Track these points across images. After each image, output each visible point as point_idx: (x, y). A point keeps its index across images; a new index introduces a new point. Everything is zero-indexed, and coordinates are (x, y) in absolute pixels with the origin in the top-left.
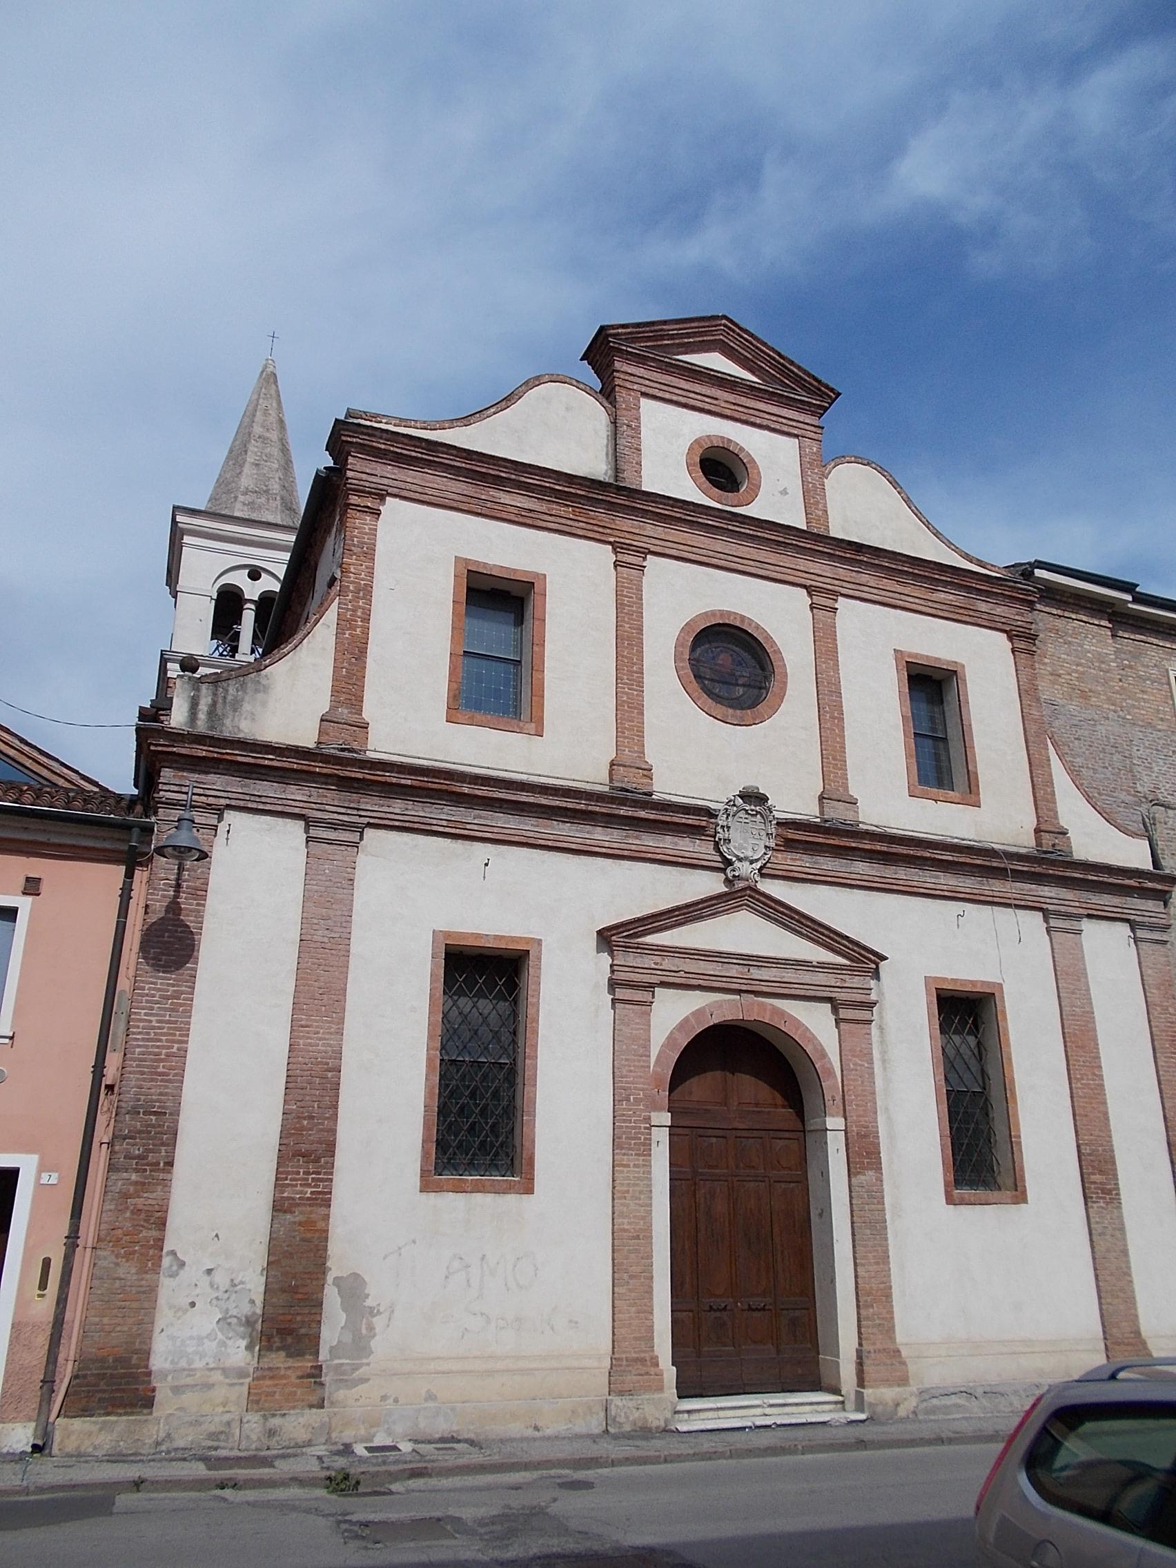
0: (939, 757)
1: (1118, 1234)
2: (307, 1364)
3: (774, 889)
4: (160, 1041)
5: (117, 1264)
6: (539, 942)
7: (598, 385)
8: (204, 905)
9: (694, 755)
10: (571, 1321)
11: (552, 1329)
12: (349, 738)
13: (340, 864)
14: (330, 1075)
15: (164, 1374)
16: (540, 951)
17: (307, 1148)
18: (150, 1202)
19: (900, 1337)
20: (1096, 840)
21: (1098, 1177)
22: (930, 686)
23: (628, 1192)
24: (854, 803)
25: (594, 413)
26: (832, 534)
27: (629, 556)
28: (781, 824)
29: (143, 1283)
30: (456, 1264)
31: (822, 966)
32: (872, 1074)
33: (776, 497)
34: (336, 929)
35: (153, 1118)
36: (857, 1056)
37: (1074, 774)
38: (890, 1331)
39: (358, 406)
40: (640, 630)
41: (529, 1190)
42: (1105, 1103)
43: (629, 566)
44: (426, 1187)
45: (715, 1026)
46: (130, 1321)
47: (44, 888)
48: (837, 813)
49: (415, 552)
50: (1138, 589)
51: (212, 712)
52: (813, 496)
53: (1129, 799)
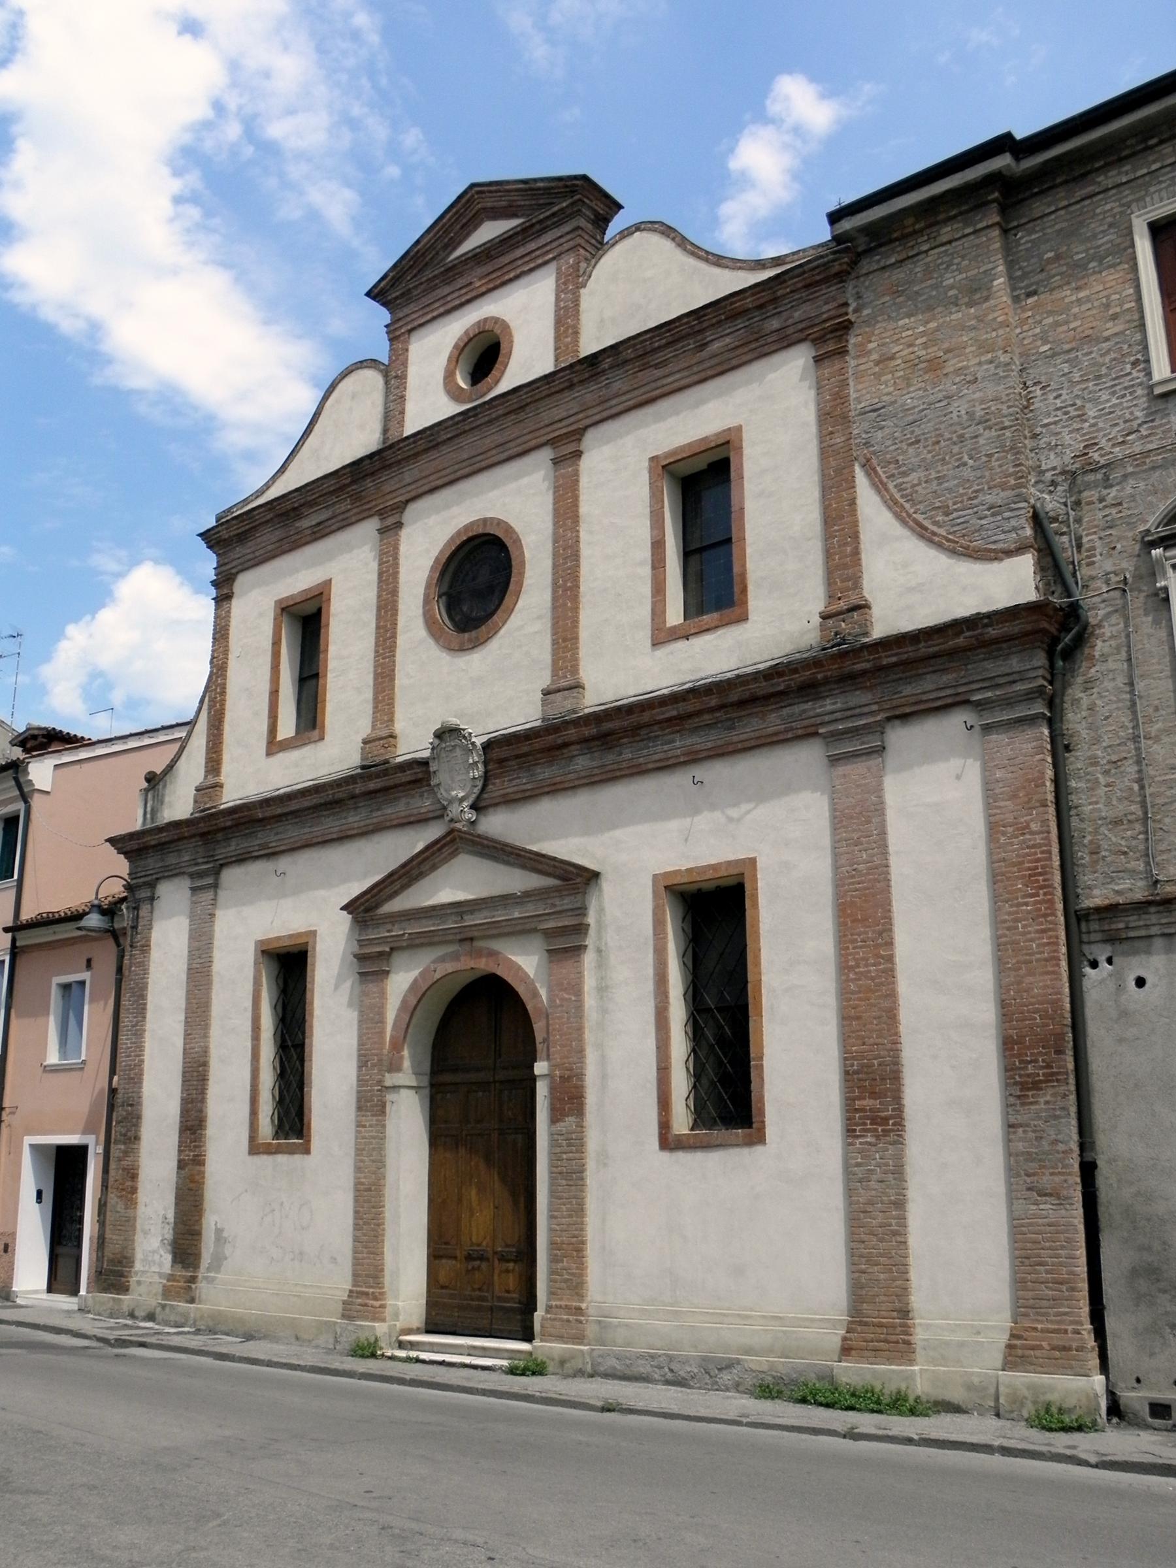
15: (136, 1273)
17: (193, 1125)
21: (873, 1098)
28: (488, 746)
51: (152, 810)
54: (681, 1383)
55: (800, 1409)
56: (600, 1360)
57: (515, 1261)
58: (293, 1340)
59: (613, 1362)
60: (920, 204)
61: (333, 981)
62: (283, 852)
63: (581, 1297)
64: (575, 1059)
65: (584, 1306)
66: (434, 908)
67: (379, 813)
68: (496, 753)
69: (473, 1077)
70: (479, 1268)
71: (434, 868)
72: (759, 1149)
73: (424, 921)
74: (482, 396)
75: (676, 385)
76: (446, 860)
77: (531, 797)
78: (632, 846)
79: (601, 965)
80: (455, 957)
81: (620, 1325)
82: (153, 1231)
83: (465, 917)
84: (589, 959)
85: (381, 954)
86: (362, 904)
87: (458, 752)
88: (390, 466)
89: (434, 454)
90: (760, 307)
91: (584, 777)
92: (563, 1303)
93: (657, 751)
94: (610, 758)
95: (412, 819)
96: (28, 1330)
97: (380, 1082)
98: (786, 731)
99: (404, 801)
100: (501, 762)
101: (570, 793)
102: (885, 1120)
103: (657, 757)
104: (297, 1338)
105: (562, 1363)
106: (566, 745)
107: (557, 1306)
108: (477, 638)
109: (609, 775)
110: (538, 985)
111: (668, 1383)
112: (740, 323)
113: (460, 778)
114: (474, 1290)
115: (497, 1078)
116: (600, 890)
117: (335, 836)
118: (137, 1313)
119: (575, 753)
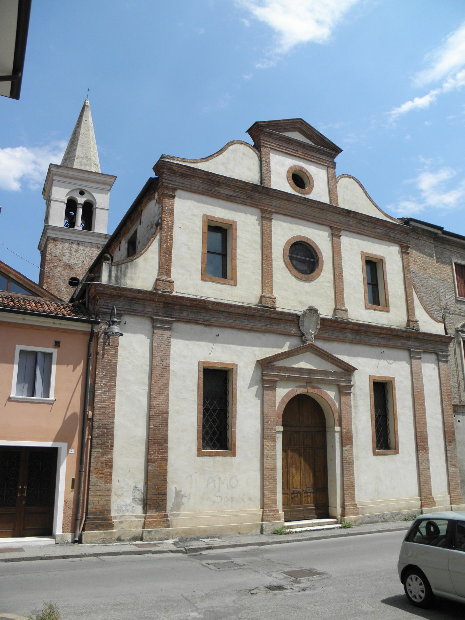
0: (375, 293)
1: (427, 462)
3: (320, 344)
4: (106, 402)
5: (97, 481)
6: (236, 365)
8: (117, 352)
9: (292, 294)
12: (167, 287)
13: (165, 336)
14: (165, 415)
16: (237, 369)
18: (107, 459)
19: (357, 500)
20: (429, 325)
22: (373, 267)
23: (268, 455)
24: (347, 311)
25: (252, 155)
26: (339, 207)
27: (266, 218)
29: (107, 487)
30: (210, 480)
32: (351, 411)
33: (319, 192)
34: (164, 361)
35: (105, 430)
37: (420, 299)
38: (353, 498)
39: (166, 153)
40: (271, 244)
41: (234, 455)
42: (425, 418)
43: (267, 218)
44: (200, 454)
45: (298, 395)
46: (103, 500)
47: (61, 344)
48: (340, 315)
49: (189, 214)
50: (444, 229)
51: (116, 277)
52: (332, 192)
53: (439, 308)
54: (386, 521)
55: (275, 536)
58: (237, 535)
59: (368, 519)
60: (430, 231)
62: (216, 326)
63: (354, 500)
67: (271, 326)
68: (325, 323)
70: (297, 496)
72: (397, 455)
73: (294, 372)
74: (303, 194)
75: (368, 234)
78: (368, 366)
79: (355, 399)
80: (305, 387)
81: (368, 507)
82: (125, 494)
84: (352, 395)
88: (268, 195)
89: (287, 203)
90: (391, 228)
94: (358, 337)
96: (111, 557)
97: (275, 429)
98: (402, 346)
99: (282, 325)
102: (425, 448)
103: (372, 342)
104: (239, 533)
105: (355, 522)
108: (308, 278)
110: (335, 401)
111: (383, 522)
112: (385, 229)
114: (295, 504)
116: (354, 376)
117: (248, 328)
118: (122, 538)
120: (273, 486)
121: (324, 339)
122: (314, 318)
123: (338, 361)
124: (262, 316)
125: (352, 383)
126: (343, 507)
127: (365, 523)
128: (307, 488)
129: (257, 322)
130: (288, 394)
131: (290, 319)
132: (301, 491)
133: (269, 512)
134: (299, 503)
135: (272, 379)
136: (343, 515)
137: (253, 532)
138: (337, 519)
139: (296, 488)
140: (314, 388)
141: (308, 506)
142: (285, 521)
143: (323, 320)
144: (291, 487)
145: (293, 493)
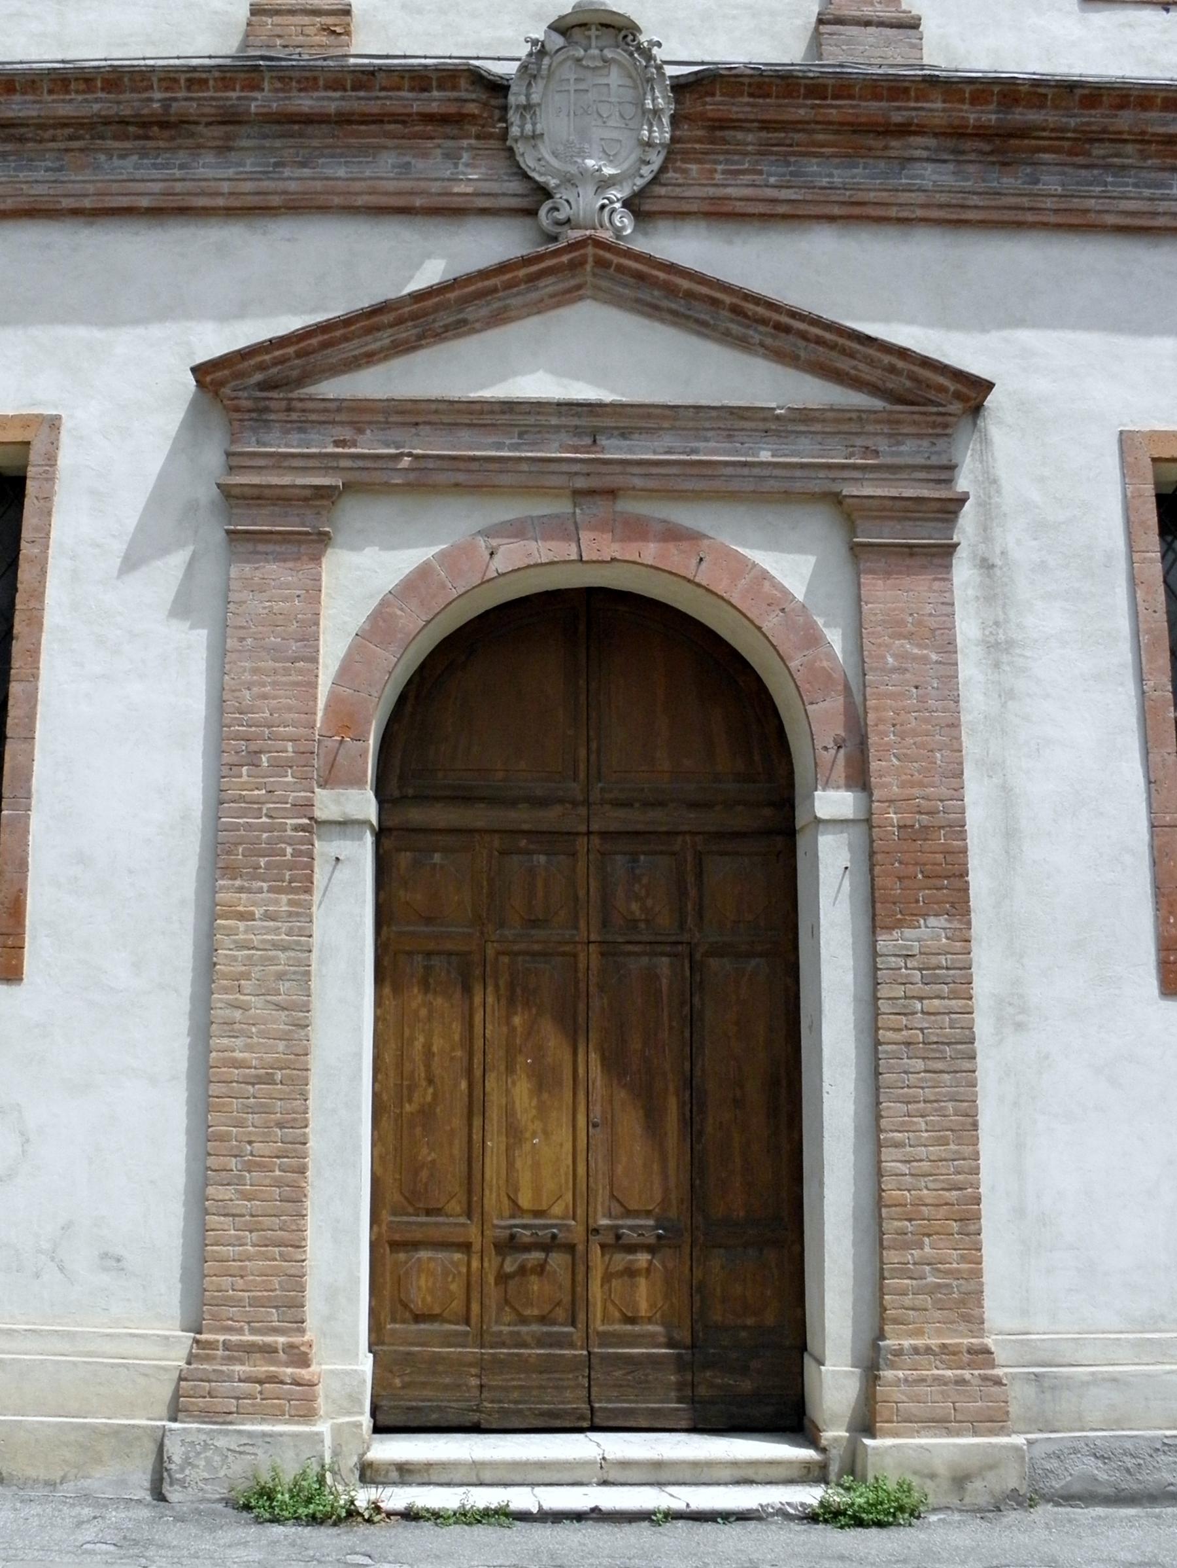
2: (500, 101)
3: (686, 248)
6: (53, 423)
7: (631, 84)
10: (105, 1256)
11: (61, 1269)
19: (1000, 1313)
23: (246, 976)
28: (680, 87)
31: (803, 417)
36: (909, 636)
38: (966, 1303)
56: (1053, 1464)
57: (651, 1249)
59: (1090, 1466)
61: (119, 547)
63: (975, 1322)
64: (944, 791)
65: (989, 1341)
66: (509, 407)
67: (306, 172)
68: (715, 105)
69: (523, 817)
70: (541, 1269)
71: (499, 319)
76: (539, 308)
77: (785, 217)
80: (568, 530)
81: (1096, 1380)
83: (603, 441)
84: (963, 571)
85: (321, 493)
86: (262, 367)
87: (614, 78)
91: (941, 206)
92: (934, 1342)
93: (1130, 196)
95: (418, 202)
100: (720, 125)
101: (892, 231)
103: (1131, 205)
105: (960, 1481)
106: (904, 130)
107: (916, 1350)
109: (1008, 216)
113: (608, 134)
114: (524, 1320)
115: (595, 827)
116: (986, 440)
119: (918, 153)
120: (278, 1183)
121: (721, 214)
122: (614, 78)
123: (819, 341)
124: (231, 119)
125: (963, 484)
126: (871, 1367)
127: (1068, 1498)
128: (628, 1213)
129: (209, 158)
130: (417, 583)
131: (434, 107)
132: (578, 1234)
133: (230, 1360)
134: (561, 1314)
135: (286, 480)
136: (866, 1423)
137: (100, 1480)
138: (824, 1450)
139: (538, 1214)
140: (637, 529)
141: (634, 1340)
142: (378, 1429)
143: (700, 86)
144: (492, 1199)
145: (509, 1245)
